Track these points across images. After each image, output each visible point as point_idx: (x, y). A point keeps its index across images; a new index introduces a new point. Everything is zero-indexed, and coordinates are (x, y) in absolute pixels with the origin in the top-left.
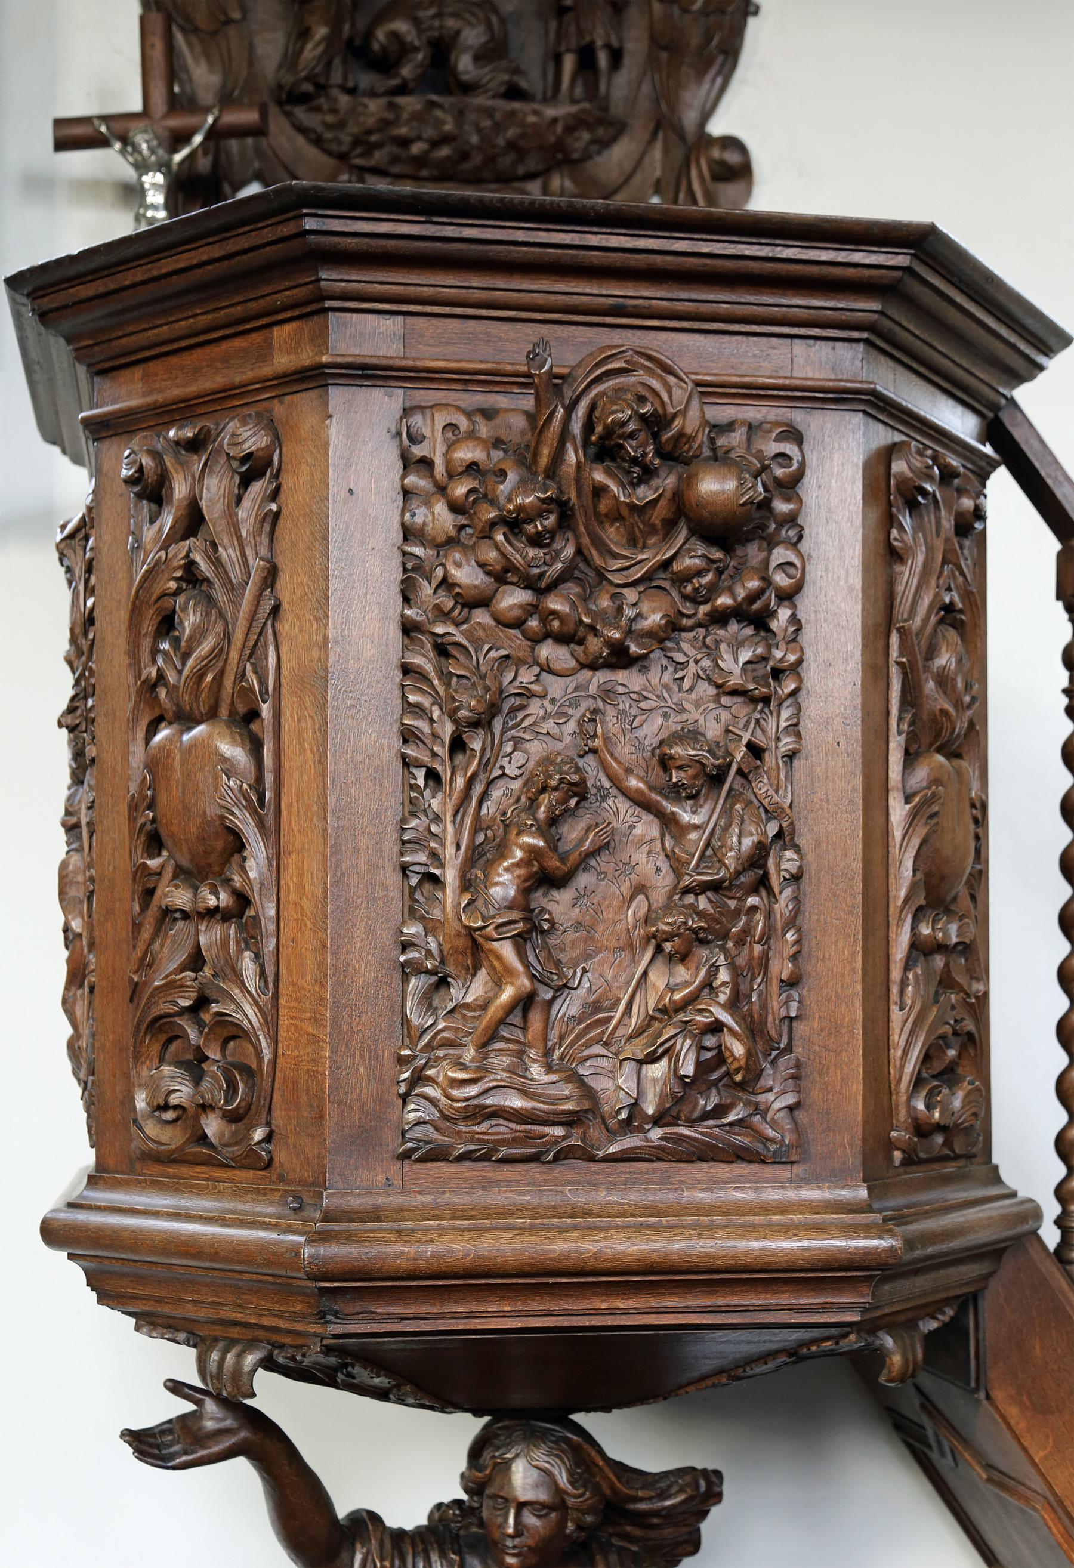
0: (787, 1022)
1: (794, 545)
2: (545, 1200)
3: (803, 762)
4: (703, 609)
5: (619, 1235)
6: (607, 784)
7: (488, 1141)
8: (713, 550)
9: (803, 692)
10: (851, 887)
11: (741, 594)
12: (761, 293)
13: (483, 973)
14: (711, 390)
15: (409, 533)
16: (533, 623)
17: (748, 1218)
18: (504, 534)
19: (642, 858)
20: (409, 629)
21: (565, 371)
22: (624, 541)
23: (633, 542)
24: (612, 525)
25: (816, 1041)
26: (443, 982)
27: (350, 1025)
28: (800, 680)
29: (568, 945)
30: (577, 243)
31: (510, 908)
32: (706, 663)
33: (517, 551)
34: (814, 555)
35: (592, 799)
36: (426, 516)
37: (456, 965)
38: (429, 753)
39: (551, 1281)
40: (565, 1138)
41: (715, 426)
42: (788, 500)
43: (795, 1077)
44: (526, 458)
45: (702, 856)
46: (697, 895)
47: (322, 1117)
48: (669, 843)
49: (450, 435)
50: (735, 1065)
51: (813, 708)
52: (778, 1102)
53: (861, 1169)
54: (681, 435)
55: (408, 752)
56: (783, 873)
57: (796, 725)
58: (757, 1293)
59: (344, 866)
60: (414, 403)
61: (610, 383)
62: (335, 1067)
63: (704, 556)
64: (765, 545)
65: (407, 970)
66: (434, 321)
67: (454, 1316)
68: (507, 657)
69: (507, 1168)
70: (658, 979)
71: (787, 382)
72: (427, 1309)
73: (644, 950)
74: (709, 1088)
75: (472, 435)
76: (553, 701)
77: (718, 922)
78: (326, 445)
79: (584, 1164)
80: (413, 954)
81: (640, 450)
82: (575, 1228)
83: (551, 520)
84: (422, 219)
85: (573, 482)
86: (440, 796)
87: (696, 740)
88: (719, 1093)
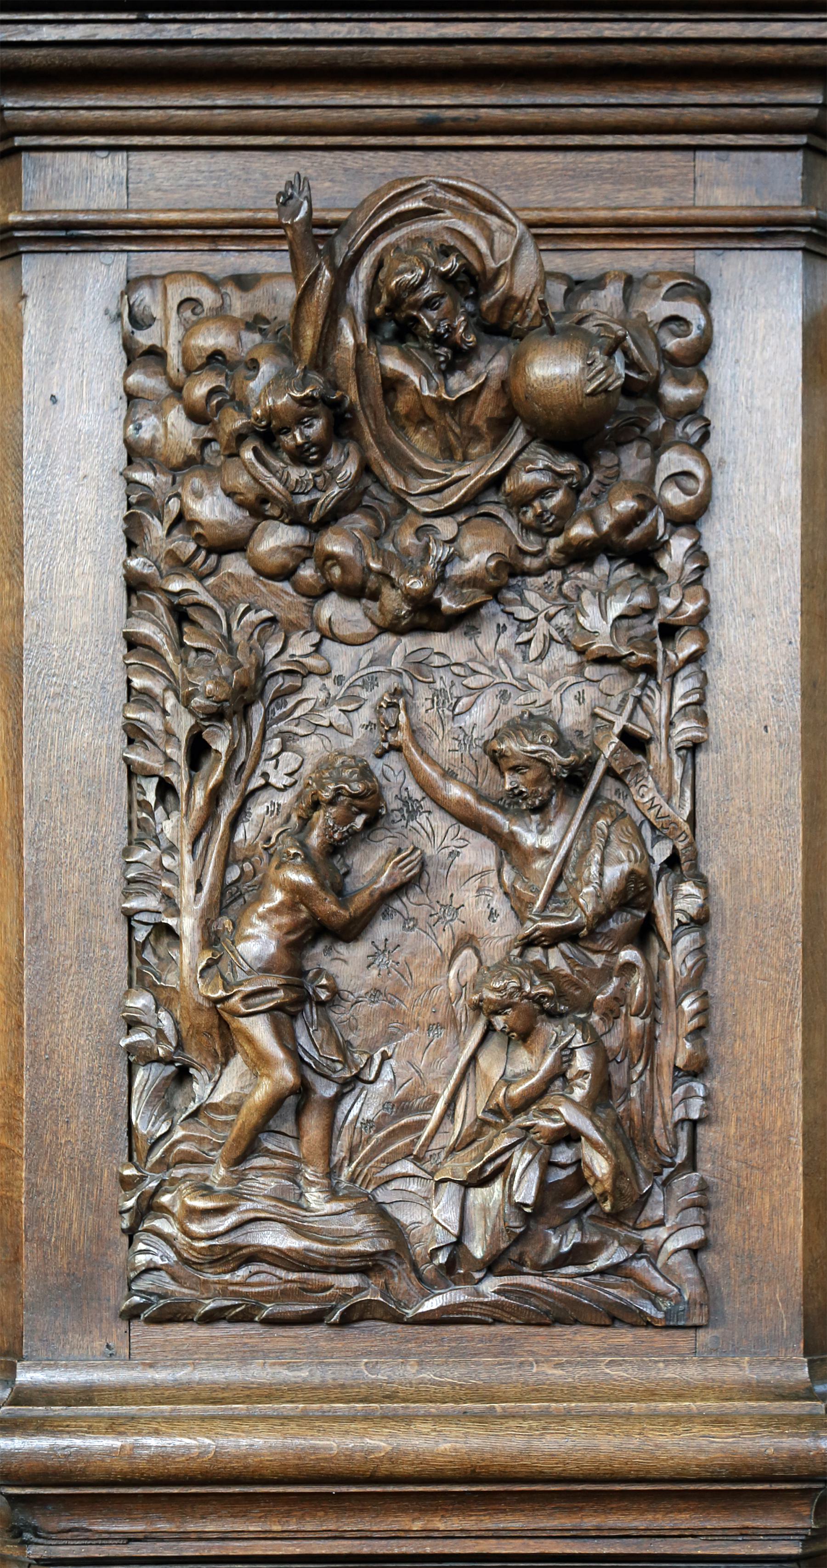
0: (686, 1126)
1: (698, 447)
2: (329, 1377)
3: (712, 755)
4: (555, 543)
5: (426, 1427)
6: (417, 794)
7: (246, 1295)
8: (561, 459)
9: (712, 656)
10: (786, 933)
11: (607, 521)
12: (639, 89)
13: (237, 1063)
14: (549, 231)
15: (135, 453)
16: (307, 572)
17: (622, 1405)
18: (255, 451)
19: (475, 899)
20: (135, 586)
21: (344, 215)
22: (437, 451)
23: (448, 453)
24: (417, 430)
25: (732, 1153)
26: (183, 1076)
27: (55, 1134)
28: (705, 638)
29: (362, 1021)
30: (356, 36)
31: (267, 970)
32: (563, 619)
33: (273, 472)
34: (729, 458)
35: (396, 816)
36: (155, 428)
37: (200, 1051)
38: (161, 758)
39: (334, 1489)
40: (358, 1290)
41: (578, 283)
42: (684, 382)
43: (702, 1206)
44: (286, 344)
45: (552, 892)
46: (546, 948)
47: (17, 1260)
48: (508, 875)
49: (188, 314)
50: (598, 1190)
51: (723, 676)
52: (674, 1240)
53: (800, 1336)
54: (508, 298)
55: (132, 756)
56: (678, 915)
57: (700, 703)
58: (642, 1512)
59: (46, 915)
60: (143, 272)
61: (404, 231)
62: (34, 1191)
63: (547, 469)
64: (648, 447)
65: (136, 1057)
66: (170, 156)
67: (201, 1537)
68: (273, 620)
69: (278, 1331)
70: (492, 1065)
71: (684, 213)
72: (163, 1526)
73: (472, 1025)
74: (567, 1222)
75: (220, 314)
76: (339, 680)
77: (577, 986)
78: (20, 336)
79: (390, 1327)
80: (139, 1037)
81: (445, 324)
82: (367, 1417)
83: (317, 428)
84: (133, 17)
85: (352, 373)
86: (175, 816)
87: (537, 729)
88: (581, 1228)
